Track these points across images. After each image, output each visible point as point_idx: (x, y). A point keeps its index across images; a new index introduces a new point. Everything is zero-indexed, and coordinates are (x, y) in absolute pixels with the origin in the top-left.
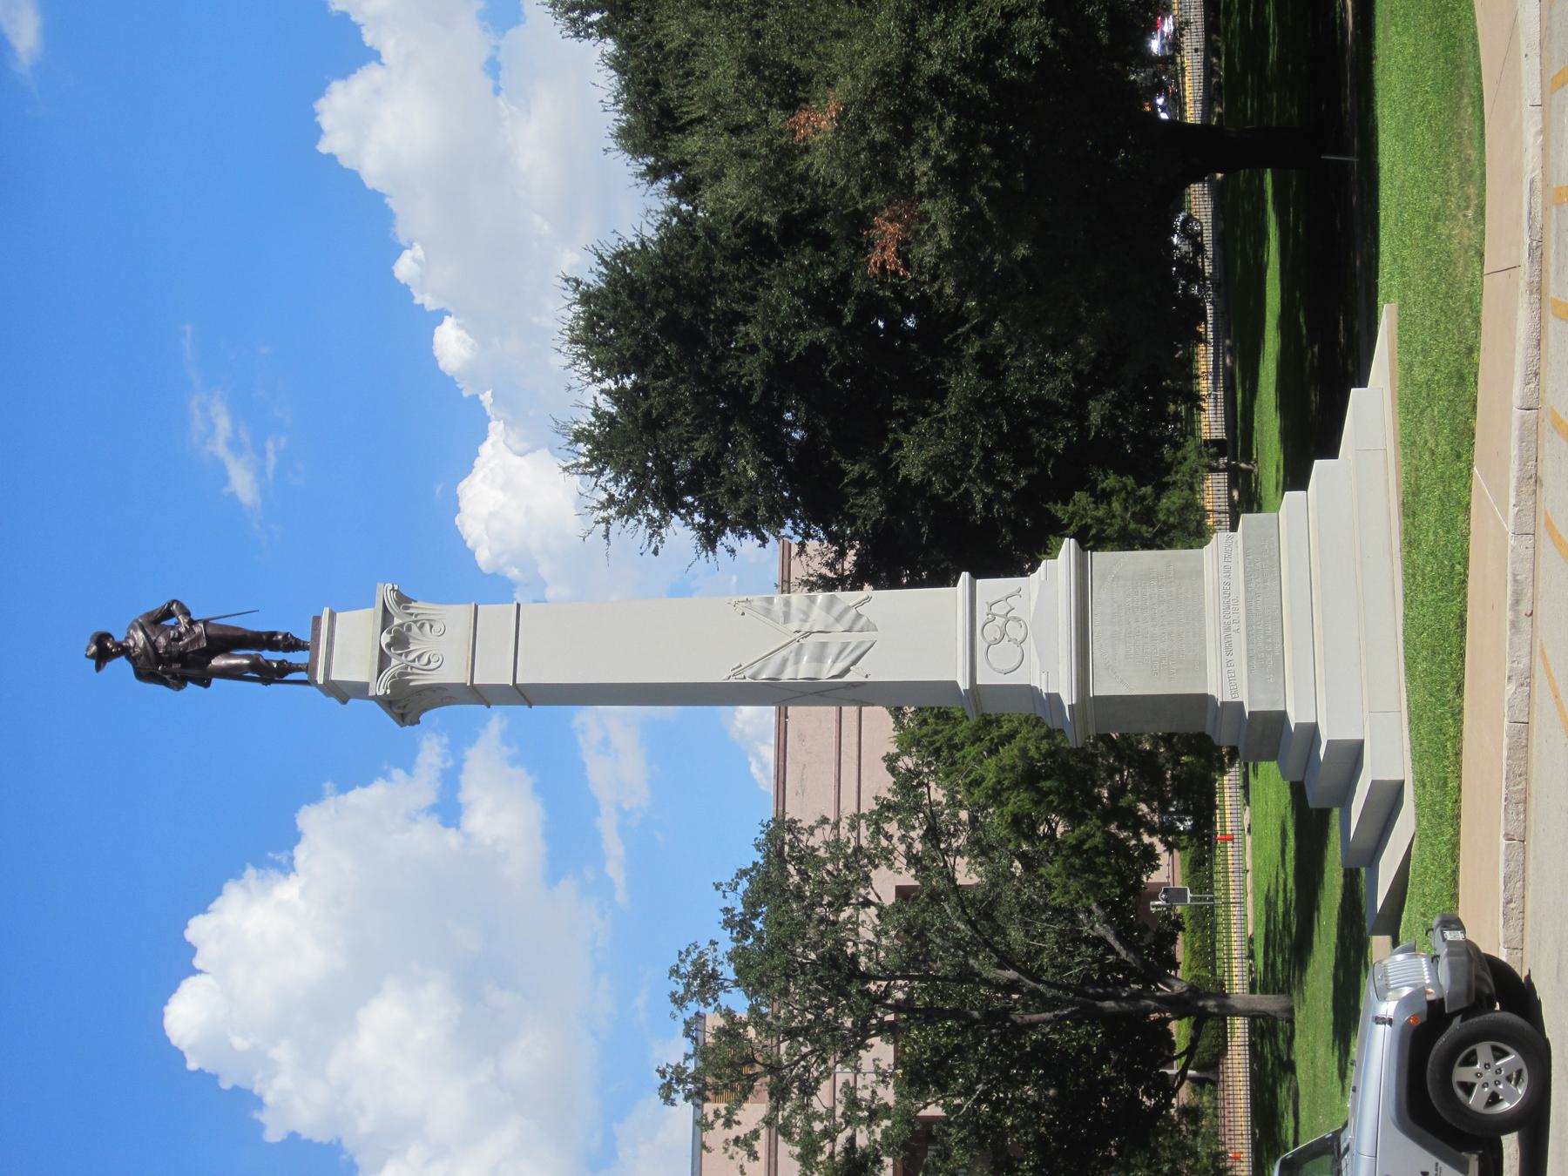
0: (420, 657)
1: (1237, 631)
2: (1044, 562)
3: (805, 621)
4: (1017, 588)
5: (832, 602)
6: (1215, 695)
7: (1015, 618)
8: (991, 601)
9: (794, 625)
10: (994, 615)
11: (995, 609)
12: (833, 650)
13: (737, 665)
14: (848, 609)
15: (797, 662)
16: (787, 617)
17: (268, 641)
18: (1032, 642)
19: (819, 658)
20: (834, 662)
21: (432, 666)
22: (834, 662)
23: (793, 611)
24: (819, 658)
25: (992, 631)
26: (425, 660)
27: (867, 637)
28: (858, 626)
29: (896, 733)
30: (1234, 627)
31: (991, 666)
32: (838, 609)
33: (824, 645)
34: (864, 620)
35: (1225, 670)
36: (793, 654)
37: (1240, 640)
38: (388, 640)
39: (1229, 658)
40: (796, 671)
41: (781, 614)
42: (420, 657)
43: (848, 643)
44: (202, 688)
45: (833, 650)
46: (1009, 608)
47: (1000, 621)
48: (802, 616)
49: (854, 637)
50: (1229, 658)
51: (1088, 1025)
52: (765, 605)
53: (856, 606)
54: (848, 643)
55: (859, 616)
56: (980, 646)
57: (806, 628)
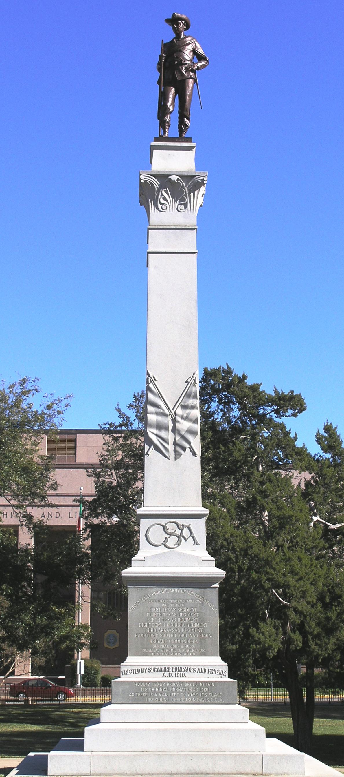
0: (165, 199)
1: (164, 676)
2: (213, 559)
3: (182, 417)
4: (199, 543)
5: (193, 433)
6: (126, 661)
7: (181, 541)
8: (191, 527)
9: (180, 411)
10: (182, 530)
11: (186, 530)
12: (163, 434)
13: (157, 379)
14: (189, 443)
15: (157, 414)
16: (185, 407)
17: (183, 113)
18: (167, 551)
19: (159, 427)
20: (156, 435)
21: (160, 206)
22: (156, 435)
23: (188, 411)
24: (159, 427)
25: (171, 527)
26: (163, 201)
27: (172, 454)
28: (178, 449)
29: (308, 452)
30: (167, 674)
31: (153, 525)
32: (190, 437)
33: (167, 429)
34: (182, 452)
35: (140, 668)
36: (162, 411)
37: (158, 677)
38: (173, 179)
39: (147, 670)
40: (151, 413)
41: (186, 404)
42: (165, 199)
43: (168, 443)
44: (157, 81)
45: (163, 434)
46: (187, 538)
47: (178, 532)
48: (185, 415)
49: (171, 447)
50: (147, 670)
51: (53, 560)
52: (193, 394)
53: (191, 448)
54: (168, 443)
55: (184, 449)
56: (163, 521)
57: (178, 419)
